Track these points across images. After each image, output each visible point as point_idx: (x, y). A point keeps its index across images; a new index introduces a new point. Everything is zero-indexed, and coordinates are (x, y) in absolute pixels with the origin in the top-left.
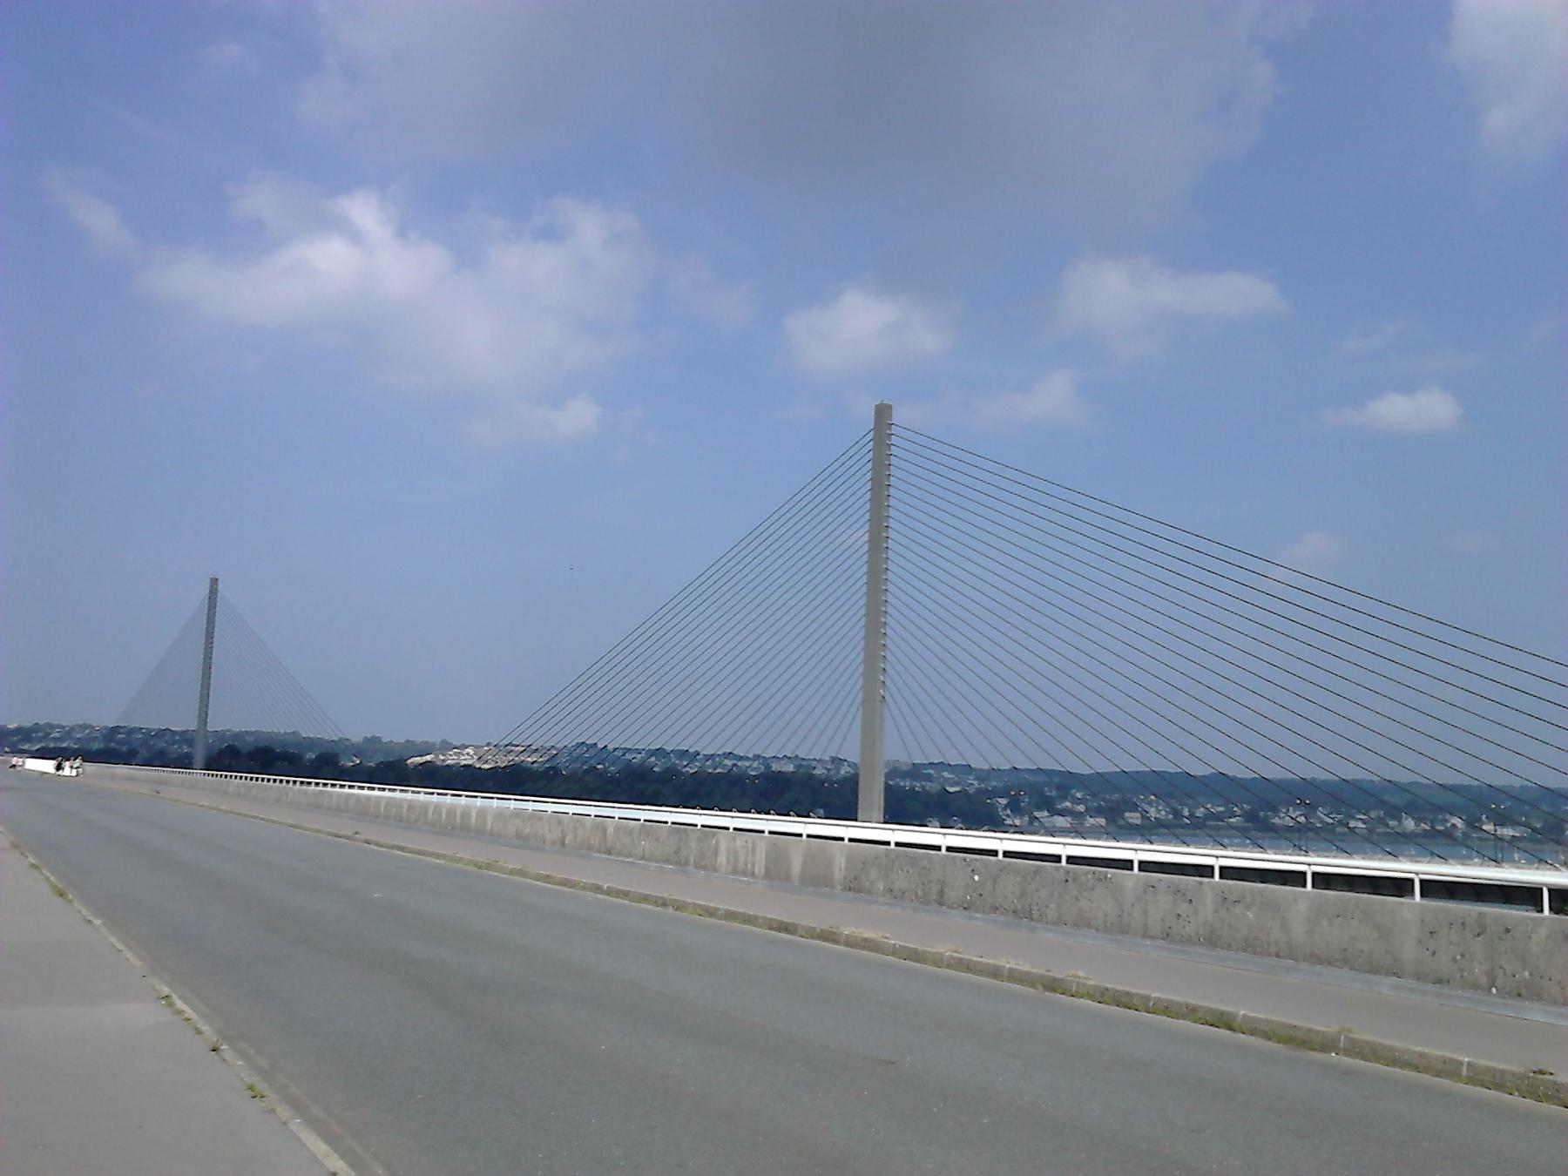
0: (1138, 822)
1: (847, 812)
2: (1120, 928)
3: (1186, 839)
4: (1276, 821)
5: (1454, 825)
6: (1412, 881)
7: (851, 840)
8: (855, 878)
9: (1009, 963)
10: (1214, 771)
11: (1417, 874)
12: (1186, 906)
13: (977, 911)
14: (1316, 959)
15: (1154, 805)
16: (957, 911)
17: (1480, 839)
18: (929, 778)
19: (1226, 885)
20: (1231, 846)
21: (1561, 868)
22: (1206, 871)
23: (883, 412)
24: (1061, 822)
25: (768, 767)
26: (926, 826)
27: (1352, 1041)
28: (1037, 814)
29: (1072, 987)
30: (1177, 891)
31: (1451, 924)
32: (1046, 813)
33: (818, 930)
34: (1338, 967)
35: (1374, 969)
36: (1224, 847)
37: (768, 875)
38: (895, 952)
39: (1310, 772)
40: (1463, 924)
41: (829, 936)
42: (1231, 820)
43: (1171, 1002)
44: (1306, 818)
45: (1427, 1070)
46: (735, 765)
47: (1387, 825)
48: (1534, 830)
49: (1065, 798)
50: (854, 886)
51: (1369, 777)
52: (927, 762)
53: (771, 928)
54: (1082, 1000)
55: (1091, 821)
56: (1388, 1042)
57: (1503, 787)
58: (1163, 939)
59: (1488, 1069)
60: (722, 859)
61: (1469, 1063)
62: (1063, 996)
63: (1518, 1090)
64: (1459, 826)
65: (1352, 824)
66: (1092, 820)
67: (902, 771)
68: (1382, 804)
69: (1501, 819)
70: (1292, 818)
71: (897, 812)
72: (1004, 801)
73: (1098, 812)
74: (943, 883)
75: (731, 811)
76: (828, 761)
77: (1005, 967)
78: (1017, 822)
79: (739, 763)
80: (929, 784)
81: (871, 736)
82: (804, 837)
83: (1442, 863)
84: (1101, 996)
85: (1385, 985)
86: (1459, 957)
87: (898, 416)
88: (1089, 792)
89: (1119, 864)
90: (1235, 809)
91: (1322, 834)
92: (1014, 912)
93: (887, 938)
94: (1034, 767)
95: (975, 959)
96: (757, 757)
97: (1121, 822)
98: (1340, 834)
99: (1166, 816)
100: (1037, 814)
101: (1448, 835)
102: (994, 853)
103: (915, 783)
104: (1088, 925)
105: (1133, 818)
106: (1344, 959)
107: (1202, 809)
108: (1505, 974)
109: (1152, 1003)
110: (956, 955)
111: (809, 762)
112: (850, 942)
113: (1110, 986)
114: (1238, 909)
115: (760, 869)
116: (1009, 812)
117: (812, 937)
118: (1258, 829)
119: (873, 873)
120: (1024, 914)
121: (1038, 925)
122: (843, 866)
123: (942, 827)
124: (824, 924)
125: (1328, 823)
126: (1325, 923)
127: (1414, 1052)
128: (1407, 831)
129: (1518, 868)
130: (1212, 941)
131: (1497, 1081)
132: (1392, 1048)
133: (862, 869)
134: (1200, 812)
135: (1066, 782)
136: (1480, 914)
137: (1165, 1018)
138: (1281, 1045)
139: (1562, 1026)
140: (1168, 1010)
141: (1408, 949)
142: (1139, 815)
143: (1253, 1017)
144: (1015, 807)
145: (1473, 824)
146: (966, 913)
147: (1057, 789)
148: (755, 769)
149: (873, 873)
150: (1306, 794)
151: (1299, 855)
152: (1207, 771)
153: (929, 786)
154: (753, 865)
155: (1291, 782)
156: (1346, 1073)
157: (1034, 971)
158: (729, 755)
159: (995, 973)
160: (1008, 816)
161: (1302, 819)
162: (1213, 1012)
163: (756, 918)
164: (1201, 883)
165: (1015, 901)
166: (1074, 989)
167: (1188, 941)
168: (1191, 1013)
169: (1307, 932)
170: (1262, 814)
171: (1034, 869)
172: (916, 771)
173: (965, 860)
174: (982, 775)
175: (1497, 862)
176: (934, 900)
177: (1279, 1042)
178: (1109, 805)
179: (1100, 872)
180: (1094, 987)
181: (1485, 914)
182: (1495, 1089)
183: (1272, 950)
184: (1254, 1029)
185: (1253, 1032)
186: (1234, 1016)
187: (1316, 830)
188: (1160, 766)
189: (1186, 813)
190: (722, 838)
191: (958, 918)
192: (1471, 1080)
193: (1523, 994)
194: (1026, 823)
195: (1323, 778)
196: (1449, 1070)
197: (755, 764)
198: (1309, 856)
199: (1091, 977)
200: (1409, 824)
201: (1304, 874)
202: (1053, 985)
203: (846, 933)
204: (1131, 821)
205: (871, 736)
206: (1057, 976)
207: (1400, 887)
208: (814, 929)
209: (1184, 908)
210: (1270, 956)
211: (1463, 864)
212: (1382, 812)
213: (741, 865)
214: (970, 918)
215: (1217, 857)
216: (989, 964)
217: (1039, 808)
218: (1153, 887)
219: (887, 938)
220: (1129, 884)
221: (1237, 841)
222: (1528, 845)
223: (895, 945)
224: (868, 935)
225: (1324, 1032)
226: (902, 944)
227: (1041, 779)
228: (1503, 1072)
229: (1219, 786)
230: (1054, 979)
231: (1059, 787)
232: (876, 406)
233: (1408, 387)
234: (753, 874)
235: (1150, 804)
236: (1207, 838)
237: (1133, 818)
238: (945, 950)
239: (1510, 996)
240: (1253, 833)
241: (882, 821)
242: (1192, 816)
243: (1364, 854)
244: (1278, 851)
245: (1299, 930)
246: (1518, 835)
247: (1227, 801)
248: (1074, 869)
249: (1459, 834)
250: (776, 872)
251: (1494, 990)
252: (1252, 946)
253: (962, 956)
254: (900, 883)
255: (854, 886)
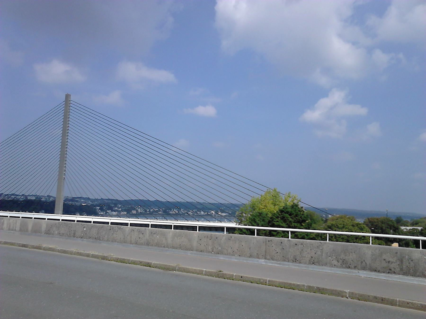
0: (136, 213)
1: (52, 212)
2: (124, 242)
3: (167, 218)
4: (171, 212)
5: (212, 213)
6: (197, 227)
7: (48, 219)
8: (49, 230)
9: (92, 252)
10: (166, 201)
11: (198, 225)
12: (141, 235)
13: (85, 239)
14: (173, 247)
15: (140, 208)
16: (79, 239)
17: (218, 216)
18: (77, 201)
19: (152, 229)
20: (159, 219)
21: (234, 223)
22: (147, 225)
23: (68, 96)
24: (114, 213)
25: (26, 198)
26: (75, 215)
27: (179, 268)
28: (108, 211)
29: (109, 258)
30: (140, 231)
31: (205, 237)
32: (110, 211)
33: (35, 246)
34: (178, 249)
35: (187, 249)
36: (138, 219)
37: (21, 230)
38: (59, 251)
39: (179, 200)
40: (207, 237)
41: (39, 248)
42: (159, 212)
43: (136, 261)
44: (178, 212)
45: (196, 273)
46: (15, 198)
47: (197, 213)
48: (229, 214)
49: (116, 207)
50: (48, 232)
51: (194, 201)
52: (77, 197)
53: (19, 246)
54: (112, 262)
55: (122, 213)
56: (187, 267)
57: (224, 203)
58: (135, 244)
59: (209, 272)
60: (5, 226)
61: (205, 270)
62: (107, 261)
63: (215, 276)
64: (213, 213)
65: (189, 213)
66: (123, 213)
67: (69, 199)
68: (196, 208)
69: (223, 212)
70: (175, 212)
71: (67, 210)
72: (99, 208)
73: (125, 210)
74: (75, 231)
75: (7, 211)
76: (46, 196)
77: (90, 254)
78: (102, 213)
79: (17, 197)
80: (77, 203)
81: (59, 189)
82: (33, 218)
83: (209, 222)
84: (117, 260)
85: (189, 253)
86: (206, 245)
87: (72, 98)
88: (122, 205)
89: (114, 224)
90: (161, 209)
91: (182, 216)
92: (95, 238)
93: (56, 247)
94: (108, 198)
95: (82, 252)
96: (23, 195)
97: (131, 213)
98: (186, 216)
99: (143, 211)
100: (108, 211)
101: (211, 215)
102: (74, 221)
103: (72, 203)
104: (116, 241)
105: (134, 212)
106: (181, 247)
107: (152, 209)
108: (216, 248)
109: (130, 261)
110: (77, 251)
111: (40, 197)
112: (45, 249)
113: (119, 257)
114: (155, 236)
115: (18, 229)
116: (100, 211)
117: (33, 248)
118: (166, 215)
119: (54, 229)
120: (98, 239)
121: (102, 242)
122: (45, 227)
123: (80, 215)
124: (36, 244)
125: (183, 213)
126: (176, 238)
127: (193, 269)
128: (202, 214)
129: (225, 223)
130: (148, 244)
131: (210, 274)
132: (188, 269)
133: (51, 227)
134: (151, 210)
135: (116, 202)
136: (211, 234)
137: (134, 265)
138: (162, 270)
139: (227, 260)
140: (134, 263)
141: (195, 244)
142: (136, 211)
143: (156, 263)
144: (102, 209)
145: (217, 213)
146: (82, 239)
147: (277, 212)
148: (22, 199)
149: (54, 229)
150: (178, 205)
151: (176, 221)
152: (154, 200)
153: (77, 203)
154: (16, 227)
155: (174, 202)
156: (177, 276)
157: (99, 254)
158: (13, 194)
159: (88, 256)
160: (99, 212)
161: (177, 212)
162: (146, 263)
163: (15, 243)
164: (146, 229)
165: (96, 235)
166: (110, 259)
167: (142, 244)
168: (141, 263)
169: (172, 241)
170: (167, 211)
171: (101, 226)
172: (73, 199)
173: (82, 224)
174: (93, 201)
175: (221, 221)
176: (72, 236)
177: (162, 269)
178: (128, 208)
179: (119, 227)
180: (115, 258)
181: (212, 234)
182: (210, 276)
183: (163, 246)
184: (156, 267)
185: (156, 267)
186: (151, 263)
187: (180, 215)
188: (142, 198)
189: (148, 210)
190: (5, 220)
191: (79, 241)
192: (205, 275)
193: (219, 253)
194: (104, 214)
195: (183, 201)
196: (200, 273)
197: (22, 197)
198: (168, 221)
199: (114, 255)
200: (202, 213)
201: (172, 225)
202: (104, 258)
203: (44, 246)
204: (133, 213)
205: (59, 189)
206: (105, 255)
207: (193, 228)
208: (34, 246)
209: (141, 236)
210: (162, 247)
211: (213, 222)
212: (196, 210)
213: (11, 228)
214: (83, 240)
215: (150, 222)
216: (86, 253)
217: (109, 210)
218: (133, 230)
219: (56, 247)
220: (127, 230)
221: (161, 218)
222: (228, 217)
223: (59, 249)
224: (50, 247)
225: (173, 266)
226: (61, 249)
227: (110, 201)
228: (212, 272)
229: (157, 203)
230: (104, 256)
231: (114, 204)
232: (66, 94)
233: (204, 104)
234: (15, 230)
235: (139, 208)
236: (153, 217)
237: (134, 212)
238: (74, 250)
239: (216, 254)
240: (165, 216)
241: (62, 214)
242: (149, 211)
243: (191, 220)
244: (170, 220)
245: (170, 241)
246: (226, 215)
247: (159, 208)
248: (112, 226)
249: (213, 215)
250: (23, 230)
251: (213, 253)
252: (158, 245)
253: (79, 251)
254: (62, 231)
255: (48, 232)
